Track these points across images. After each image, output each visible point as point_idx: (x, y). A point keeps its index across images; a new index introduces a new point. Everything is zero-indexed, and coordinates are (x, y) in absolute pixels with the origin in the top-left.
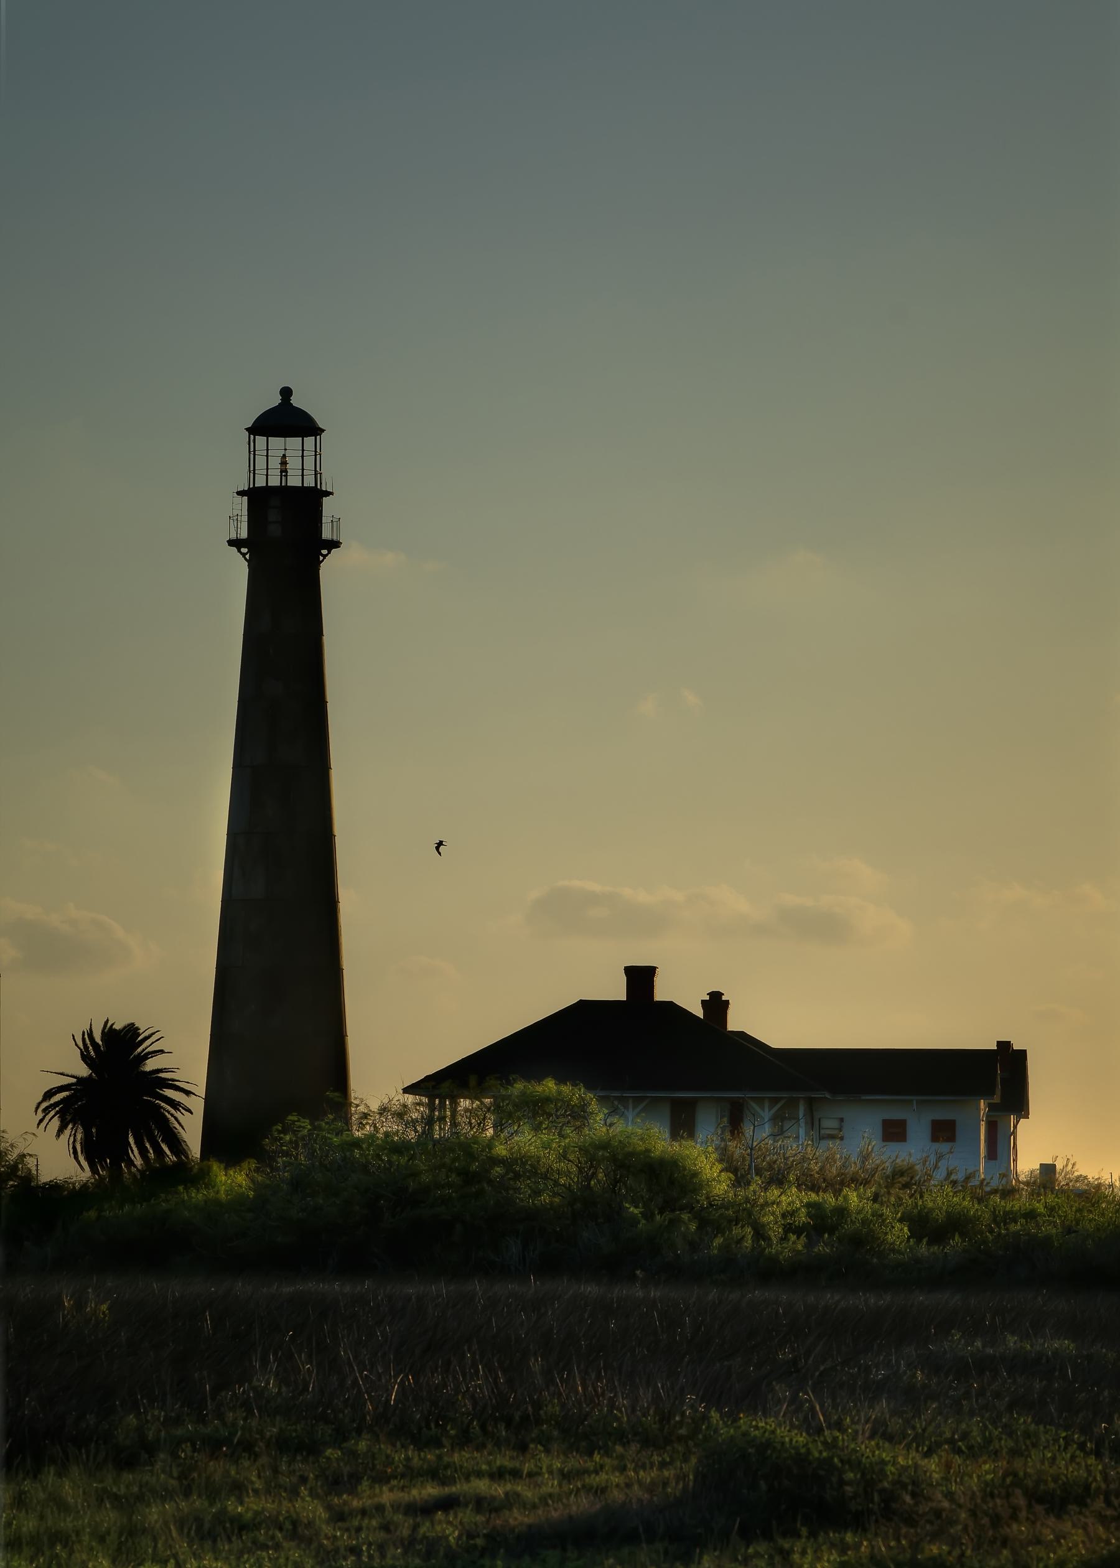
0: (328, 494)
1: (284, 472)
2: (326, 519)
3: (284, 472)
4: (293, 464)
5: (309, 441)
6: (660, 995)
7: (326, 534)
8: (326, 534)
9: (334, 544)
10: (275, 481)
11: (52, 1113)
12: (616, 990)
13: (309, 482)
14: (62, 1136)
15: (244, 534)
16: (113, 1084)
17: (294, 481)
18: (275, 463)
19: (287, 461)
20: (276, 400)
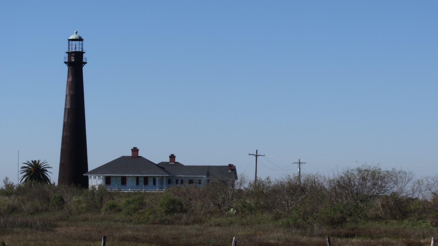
0: (84, 53)
1: (76, 48)
2: (84, 58)
3: (76, 48)
4: (77, 46)
5: (81, 42)
6: (139, 155)
7: (84, 61)
8: (84, 61)
9: (85, 63)
10: (74, 50)
11: (25, 169)
12: (130, 154)
13: (81, 50)
14: (140, 183)
15: (67, 61)
16: (36, 172)
17: (77, 50)
18: (74, 47)
19: (76, 47)
20: (67, 54)
